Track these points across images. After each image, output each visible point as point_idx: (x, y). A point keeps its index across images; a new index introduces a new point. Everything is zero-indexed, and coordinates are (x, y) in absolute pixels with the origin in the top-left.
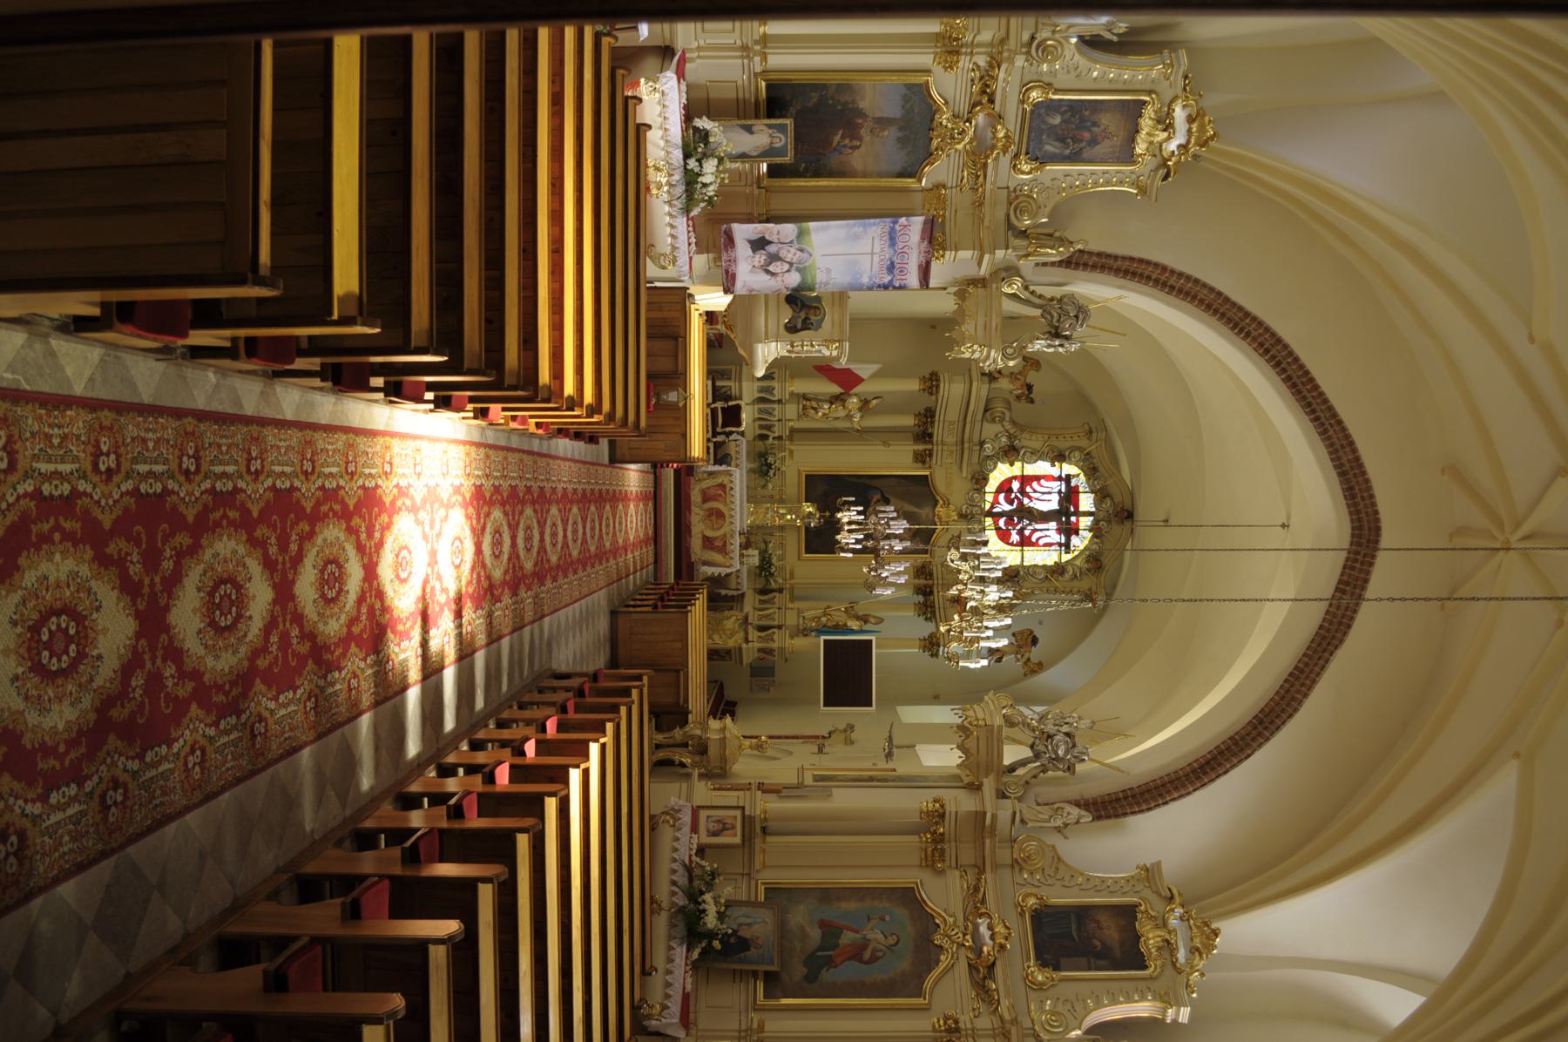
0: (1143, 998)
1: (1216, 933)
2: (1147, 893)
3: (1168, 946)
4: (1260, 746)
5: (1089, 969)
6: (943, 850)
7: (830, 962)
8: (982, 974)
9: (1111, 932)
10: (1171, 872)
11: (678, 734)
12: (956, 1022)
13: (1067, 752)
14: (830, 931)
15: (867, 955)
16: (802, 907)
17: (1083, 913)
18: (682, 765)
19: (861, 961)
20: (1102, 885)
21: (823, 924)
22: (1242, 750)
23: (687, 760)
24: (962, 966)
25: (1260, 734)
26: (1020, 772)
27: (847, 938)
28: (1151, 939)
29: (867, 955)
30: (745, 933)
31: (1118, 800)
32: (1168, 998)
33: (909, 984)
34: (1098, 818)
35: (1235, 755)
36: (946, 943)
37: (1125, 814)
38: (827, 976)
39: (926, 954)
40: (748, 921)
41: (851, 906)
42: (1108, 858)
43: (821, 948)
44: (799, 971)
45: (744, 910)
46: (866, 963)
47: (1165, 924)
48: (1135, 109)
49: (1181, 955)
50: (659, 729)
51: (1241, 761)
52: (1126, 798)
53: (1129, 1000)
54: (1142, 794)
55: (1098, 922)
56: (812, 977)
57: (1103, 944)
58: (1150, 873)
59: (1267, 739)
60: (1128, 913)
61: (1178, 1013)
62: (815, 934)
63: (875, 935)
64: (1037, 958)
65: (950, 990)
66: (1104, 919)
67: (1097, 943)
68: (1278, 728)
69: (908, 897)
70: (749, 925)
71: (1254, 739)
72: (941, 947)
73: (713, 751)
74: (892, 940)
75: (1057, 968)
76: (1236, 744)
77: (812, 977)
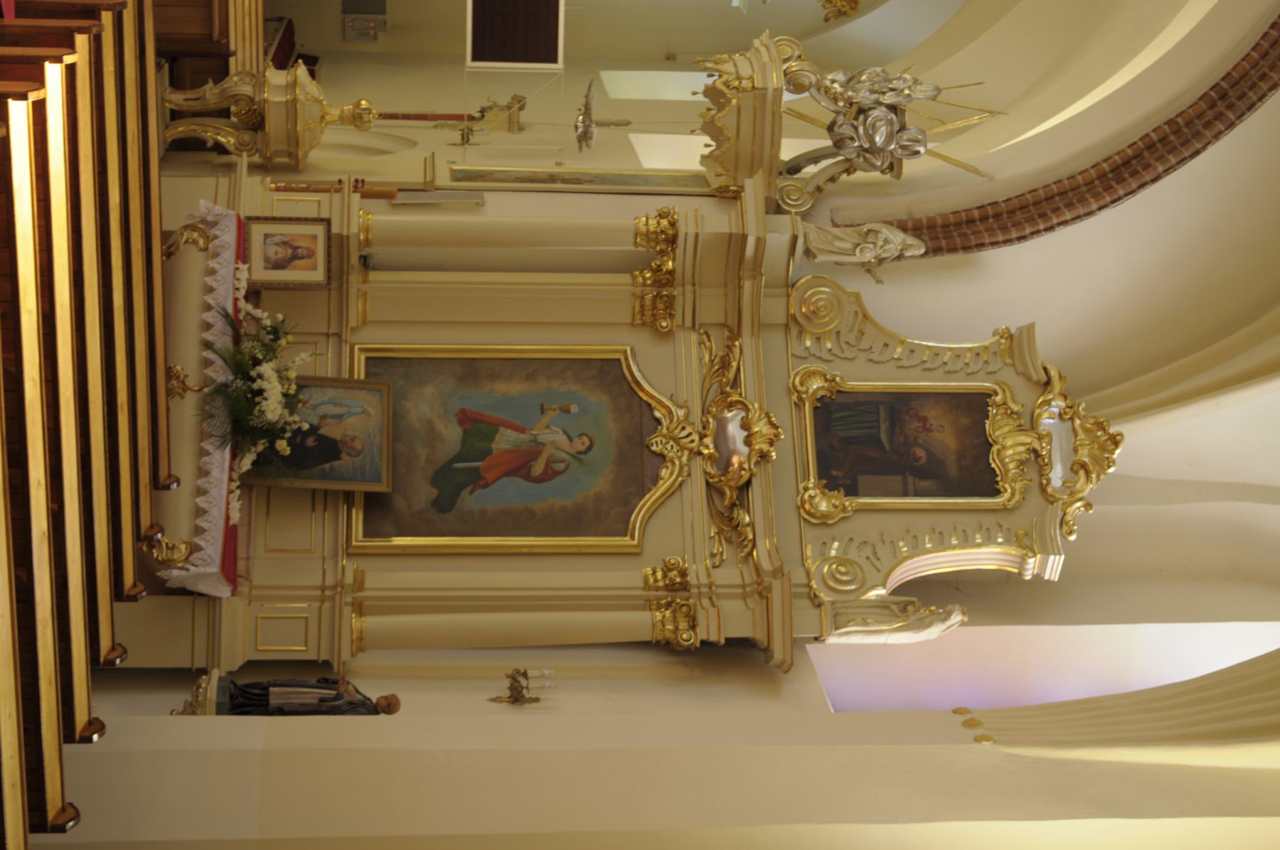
0: (989, 540)
1: (1115, 441)
2: (1008, 375)
3: (1036, 460)
4: (1217, 136)
5: (905, 494)
6: (671, 298)
7: (477, 480)
8: (729, 499)
9: (944, 436)
10: (1049, 346)
11: (210, 93)
12: (683, 574)
13: (890, 138)
14: (477, 428)
15: (538, 468)
16: (429, 390)
17: (900, 405)
18: (220, 149)
19: (528, 477)
20: (935, 361)
21: (465, 418)
22: (1186, 143)
23: (228, 140)
24: (696, 488)
25: (1219, 116)
26: (810, 170)
27: (505, 440)
28: (1009, 446)
29: (538, 468)
30: (331, 430)
31: (971, 222)
32: (1028, 542)
33: (607, 516)
34: (935, 251)
35: (1173, 150)
36: (671, 450)
37: (981, 246)
38: (471, 500)
39: (637, 466)
40: (338, 410)
41: (515, 388)
42: (944, 317)
43: (460, 457)
44: (423, 493)
45: (331, 393)
46: (540, 480)
47: (1033, 425)
48: (671, 316)
49: (1057, 476)
50: (176, 83)
51: (1182, 161)
52: (984, 219)
53: (966, 542)
54: (1011, 213)
55: (924, 420)
56: (444, 504)
57: (931, 455)
58: (1014, 344)
59: (1231, 125)
60: (973, 406)
61: (1043, 565)
62: (452, 434)
63: (553, 436)
64: (821, 474)
65: (675, 525)
66: (933, 414)
67: (920, 453)
68: (1251, 107)
69: (609, 374)
70: (339, 417)
71: (1207, 125)
72: (662, 456)
73: (274, 123)
74: (580, 445)
75: (852, 491)
76: (1177, 132)
77: (444, 504)
